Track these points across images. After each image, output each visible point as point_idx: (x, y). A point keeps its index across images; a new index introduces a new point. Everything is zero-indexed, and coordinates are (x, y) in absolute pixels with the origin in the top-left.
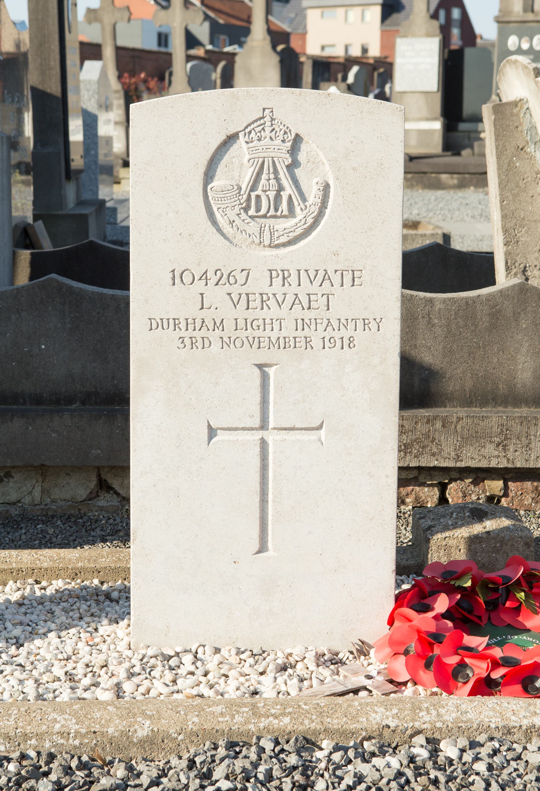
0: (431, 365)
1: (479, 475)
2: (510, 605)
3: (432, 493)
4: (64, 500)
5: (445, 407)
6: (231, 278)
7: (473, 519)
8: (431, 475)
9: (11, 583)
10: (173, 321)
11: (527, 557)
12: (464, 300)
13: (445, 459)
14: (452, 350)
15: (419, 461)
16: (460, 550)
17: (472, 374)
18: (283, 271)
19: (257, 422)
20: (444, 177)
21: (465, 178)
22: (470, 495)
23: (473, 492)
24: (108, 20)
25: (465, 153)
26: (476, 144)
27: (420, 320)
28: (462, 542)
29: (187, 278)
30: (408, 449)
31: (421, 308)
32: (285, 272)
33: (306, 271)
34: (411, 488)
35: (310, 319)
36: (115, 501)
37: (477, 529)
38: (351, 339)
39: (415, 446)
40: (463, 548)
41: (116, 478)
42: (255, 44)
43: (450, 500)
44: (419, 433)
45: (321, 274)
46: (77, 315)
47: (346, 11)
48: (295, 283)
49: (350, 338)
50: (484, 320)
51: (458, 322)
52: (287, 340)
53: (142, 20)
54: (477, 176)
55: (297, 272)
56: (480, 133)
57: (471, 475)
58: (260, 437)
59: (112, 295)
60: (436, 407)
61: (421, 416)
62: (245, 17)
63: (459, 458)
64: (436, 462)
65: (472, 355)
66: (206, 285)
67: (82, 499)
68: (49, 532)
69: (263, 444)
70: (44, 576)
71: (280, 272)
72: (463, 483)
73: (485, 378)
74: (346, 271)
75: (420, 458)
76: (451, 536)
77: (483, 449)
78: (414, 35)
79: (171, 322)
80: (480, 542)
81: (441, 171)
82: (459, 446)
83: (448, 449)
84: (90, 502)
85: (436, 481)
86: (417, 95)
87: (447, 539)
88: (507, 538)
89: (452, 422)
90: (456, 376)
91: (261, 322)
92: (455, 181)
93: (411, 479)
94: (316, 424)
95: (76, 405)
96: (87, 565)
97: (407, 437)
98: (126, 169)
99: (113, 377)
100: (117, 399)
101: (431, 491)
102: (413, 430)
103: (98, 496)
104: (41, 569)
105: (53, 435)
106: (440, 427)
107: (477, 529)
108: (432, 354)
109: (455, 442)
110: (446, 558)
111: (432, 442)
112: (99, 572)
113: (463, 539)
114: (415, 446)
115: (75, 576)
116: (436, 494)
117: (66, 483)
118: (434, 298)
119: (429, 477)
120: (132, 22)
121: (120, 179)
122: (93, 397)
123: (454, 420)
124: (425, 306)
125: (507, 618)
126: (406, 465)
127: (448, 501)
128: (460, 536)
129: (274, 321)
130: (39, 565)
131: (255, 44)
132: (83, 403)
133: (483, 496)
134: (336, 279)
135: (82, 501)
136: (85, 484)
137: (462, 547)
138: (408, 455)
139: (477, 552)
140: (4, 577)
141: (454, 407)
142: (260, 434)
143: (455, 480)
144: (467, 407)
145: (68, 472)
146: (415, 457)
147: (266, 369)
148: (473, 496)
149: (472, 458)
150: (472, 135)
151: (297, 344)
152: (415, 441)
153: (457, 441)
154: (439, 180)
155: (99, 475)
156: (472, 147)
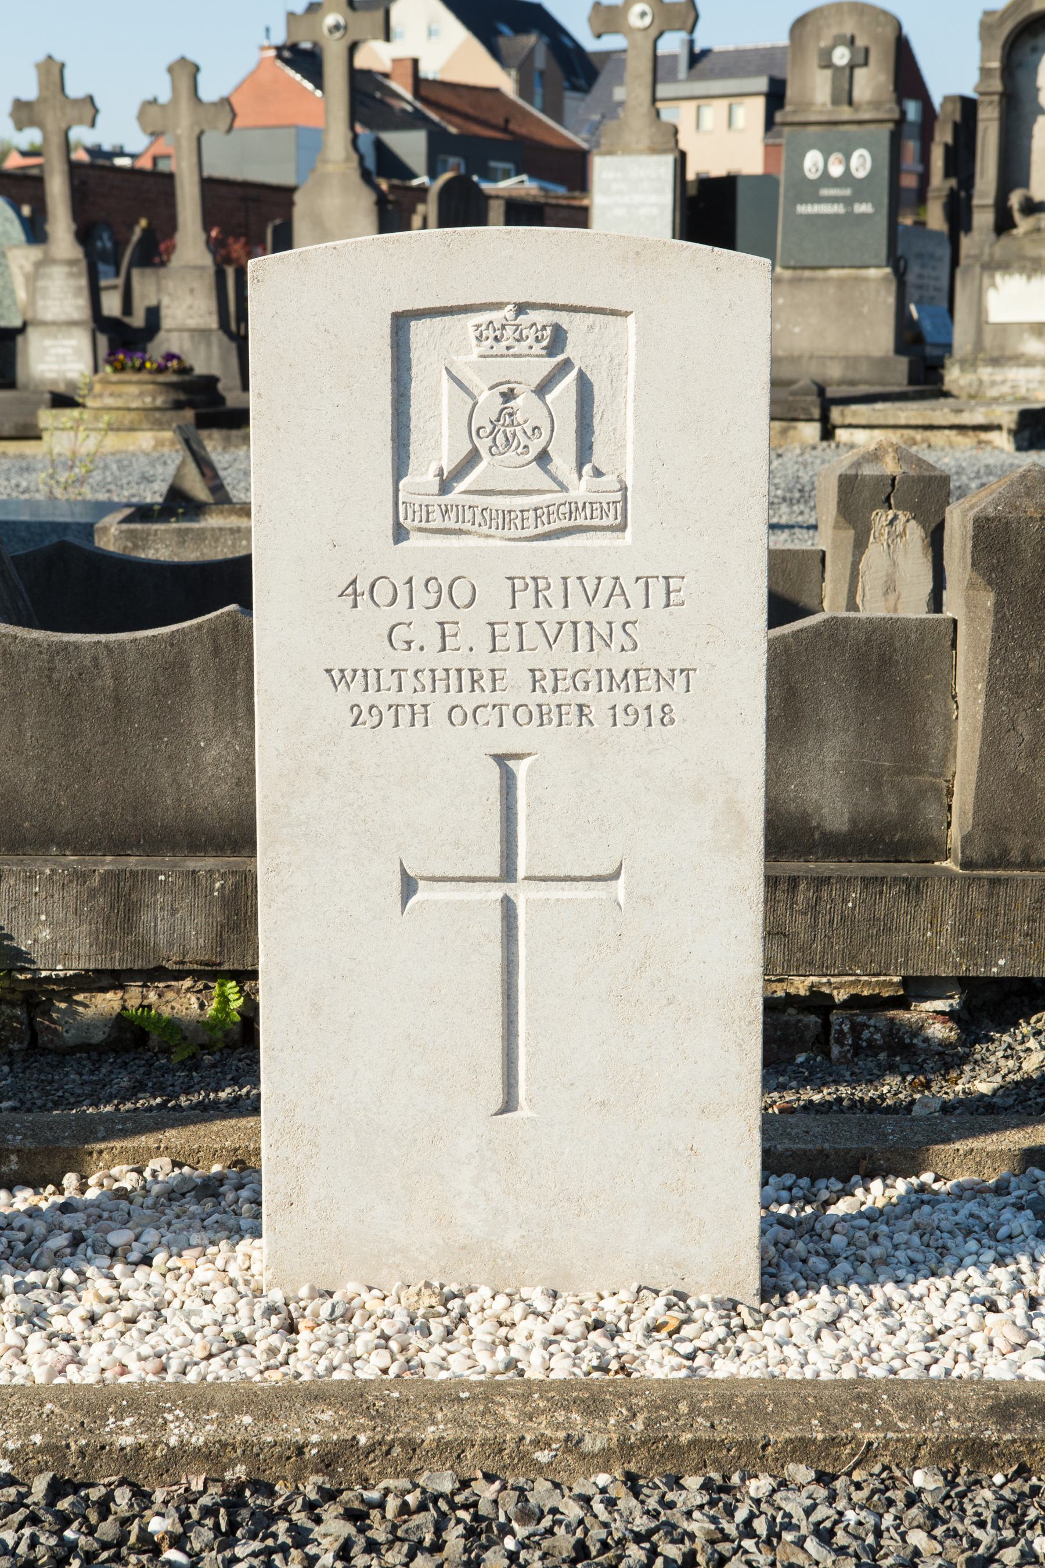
18: (535, 579)
19: (496, 872)
29: (383, 592)
35: (673, 671)
42: (330, 168)
45: (607, 585)
47: (698, 108)
48: (558, 602)
49: (664, 707)
52: (545, 709)
53: (297, 127)
55: (562, 581)
66: (355, 606)
69: (508, 907)
71: (529, 581)
74: (652, 577)
78: (628, 151)
79: (466, 674)
120: (233, 133)
121: (42, 430)
129: (677, 672)
131: (330, 168)
134: (636, 593)
142: (496, 892)
147: (511, 764)
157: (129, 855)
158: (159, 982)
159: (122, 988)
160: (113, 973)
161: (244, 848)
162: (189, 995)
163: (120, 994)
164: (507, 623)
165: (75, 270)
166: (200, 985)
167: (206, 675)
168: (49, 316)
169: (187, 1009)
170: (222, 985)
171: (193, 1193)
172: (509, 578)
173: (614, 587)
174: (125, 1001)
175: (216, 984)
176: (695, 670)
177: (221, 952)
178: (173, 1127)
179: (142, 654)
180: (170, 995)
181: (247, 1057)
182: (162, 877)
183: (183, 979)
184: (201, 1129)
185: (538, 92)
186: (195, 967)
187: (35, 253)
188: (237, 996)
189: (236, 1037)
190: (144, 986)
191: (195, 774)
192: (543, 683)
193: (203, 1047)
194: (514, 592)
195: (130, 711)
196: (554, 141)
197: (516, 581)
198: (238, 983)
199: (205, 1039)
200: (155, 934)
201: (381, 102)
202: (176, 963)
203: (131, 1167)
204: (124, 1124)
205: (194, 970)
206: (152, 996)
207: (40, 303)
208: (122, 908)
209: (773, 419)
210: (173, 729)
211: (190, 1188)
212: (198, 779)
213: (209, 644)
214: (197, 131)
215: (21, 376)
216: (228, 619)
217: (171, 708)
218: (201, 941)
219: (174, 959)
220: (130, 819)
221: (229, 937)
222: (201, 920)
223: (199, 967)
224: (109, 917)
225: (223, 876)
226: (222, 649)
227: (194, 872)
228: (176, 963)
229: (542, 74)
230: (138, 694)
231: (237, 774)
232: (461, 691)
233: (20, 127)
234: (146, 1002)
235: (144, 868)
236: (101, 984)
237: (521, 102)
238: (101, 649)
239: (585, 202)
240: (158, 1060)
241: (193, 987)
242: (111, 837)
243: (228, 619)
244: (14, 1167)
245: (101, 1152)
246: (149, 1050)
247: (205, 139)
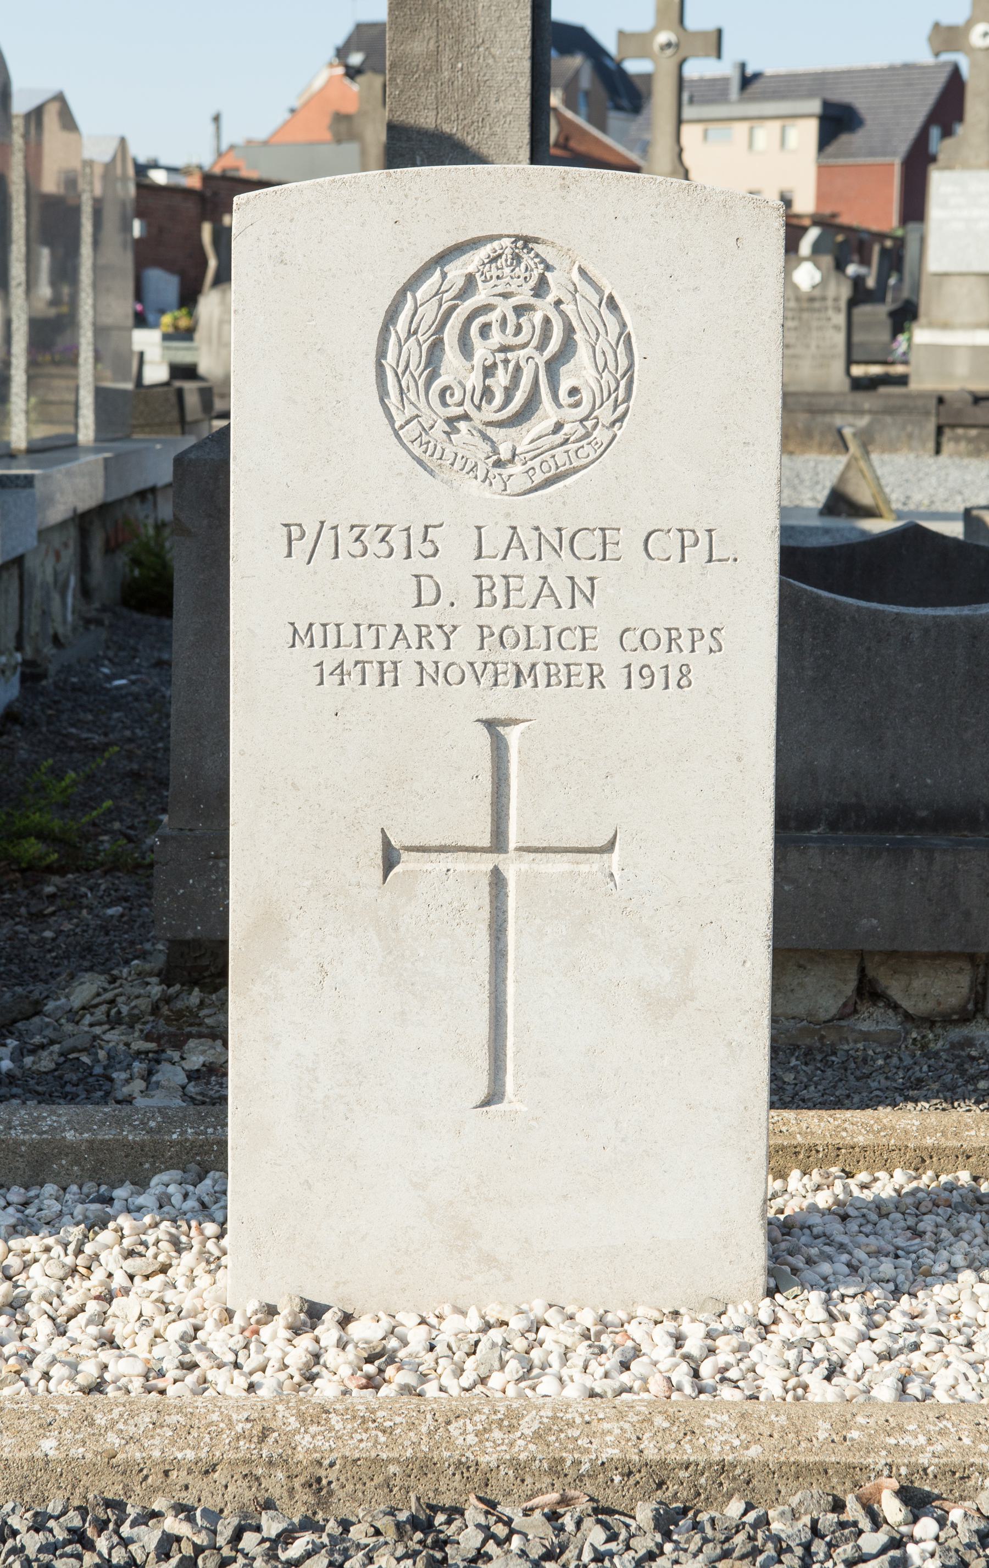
4: (793, 1018)
9: (795, 1174)
19: (486, 842)
36: (891, 1022)
41: (897, 976)
46: (828, 651)
58: (491, 867)
59: (897, 614)
67: (828, 1017)
68: (786, 1080)
69: (497, 880)
70: (858, 1162)
84: (843, 1023)
95: (820, 830)
96: (944, 1143)
99: (892, 777)
100: (899, 819)
103: (855, 1011)
104: (853, 1148)
105: (786, 888)
112: (968, 1157)
115: (919, 1164)
117: (799, 984)
122: (853, 815)
130: (848, 1140)
132: (833, 826)
135: (829, 1021)
136: (835, 985)
140: (781, 1162)
142: (486, 863)
145: (802, 962)
147: (500, 729)
151: (572, 678)
155: (862, 971)
164: (522, 577)
172: (286, 525)
173: (512, 540)
176: (385, 626)
185: (583, 109)
192: (429, 638)
194: (683, 548)
197: (292, 528)
229: (587, 94)
232: (325, 645)
239: (646, 136)
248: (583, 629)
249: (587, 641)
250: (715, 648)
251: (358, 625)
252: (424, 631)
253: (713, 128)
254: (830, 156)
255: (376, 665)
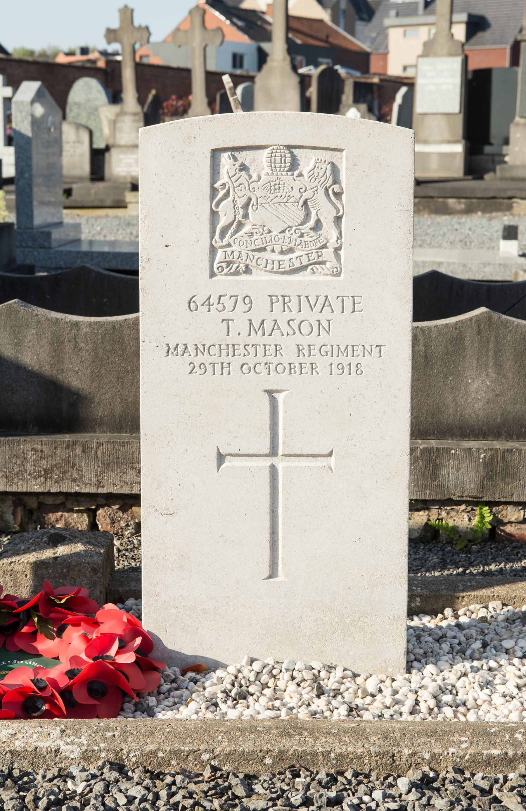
0: (79, 389)
1: (126, 501)
2: (28, 629)
3: (82, 519)
5: (95, 432)
6: (192, 304)
7: (48, 544)
8: (78, 501)
10: (351, 348)
11: (95, 583)
12: (110, 324)
13: (86, 485)
14: (100, 375)
15: (60, 486)
16: (26, 575)
17: (121, 400)
19: (267, 451)
20: (451, 202)
21: (472, 203)
22: (119, 521)
23: (121, 518)
24: (127, 39)
25: (488, 177)
26: (498, 168)
27: (67, 344)
28: (28, 567)
30: (48, 474)
31: (67, 332)
32: (273, 298)
33: (307, 297)
34: (60, 513)
37: (48, 554)
38: (359, 365)
39: (56, 472)
40: (29, 573)
42: (275, 64)
43: (100, 526)
44: (58, 458)
45: (321, 300)
49: (357, 364)
50: (132, 344)
51: (106, 346)
54: (485, 201)
56: (504, 156)
57: (118, 501)
58: (270, 464)
60: (85, 432)
61: (60, 441)
62: (324, 37)
63: (100, 483)
64: (77, 488)
65: (120, 380)
66: (209, 311)
72: (110, 509)
73: (134, 403)
75: (61, 484)
76: (17, 561)
77: (125, 475)
80: (46, 568)
81: (448, 195)
82: (100, 472)
83: (90, 475)
85: (83, 507)
86: (439, 116)
87: (12, 564)
88: (74, 564)
89: (92, 448)
90: (105, 401)
91: (329, 348)
92: (463, 206)
93: (58, 504)
94: (326, 452)
97: (47, 462)
98: (134, 194)
101: (81, 517)
102: (53, 455)
106: (80, 452)
107: (48, 554)
108: (80, 379)
109: (96, 468)
110: (12, 583)
111: (73, 467)
113: (29, 565)
114: (56, 472)
116: (85, 521)
118: (79, 322)
119: (76, 503)
121: (127, 203)
123: (95, 445)
124: (71, 330)
125: (20, 644)
126: (46, 491)
127: (98, 527)
128: (26, 561)
133: (132, 522)
134: (337, 305)
137: (28, 572)
138: (48, 480)
139: (44, 578)
141: (104, 433)
142: (267, 462)
143: (103, 506)
144: (117, 432)
146: (56, 482)
148: (122, 522)
149: (114, 484)
150: (497, 159)
152: (55, 466)
153: (98, 466)
154: (446, 205)
156: (494, 170)
157: (429, 439)
158: (448, 506)
159: (428, 509)
160: (424, 502)
161: (489, 436)
162: (463, 514)
163: (427, 512)
165: (137, 118)
166: (469, 508)
167: (473, 345)
168: (123, 142)
169: (462, 521)
170: (481, 509)
171: (519, 620)
174: (429, 516)
175: (478, 508)
177: (482, 491)
178: (497, 585)
179: (440, 333)
180: (453, 514)
181: (494, 547)
182: (453, 451)
183: (460, 505)
184: (513, 586)
185: (342, 21)
186: (468, 499)
187: (115, 109)
188: (489, 515)
189: (487, 536)
190: (440, 508)
191: (465, 397)
193: (470, 541)
195: (433, 363)
196: (353, 48)
198: (489, 507)
199: (470, 537)
200: (448, 481)
201: (261, 27)
202: (458, 497)
203: (482, 606)
204: (471, 582)
205: (468, 501)
206: (444, 514)
207: (118, 135)
208: (431, 467)
209: (415, 197)
210: (455, 373)
211: (517, 617)
212: (466, 399)
213: (475, 328)
214: (203, 45)
215: (107, 174)
216: (486, 315)
217: (454, 362)
218: (472, 485)
219: (458, 494)
220: (430, 420)
221: (487, 484)
222: (472, 474)
223: (471, 499)
224: (424, 472)
225: (485, 451)
226: (482, 331)
227: (470, 449)
228: (458, 497)
229: (344, 12)
230: (437, 354)
231: (487, 397)
233: (109, 42)
234: (440, 517)
235: (443, 446)
236: (417, 507)
237: (334, 26)
238: (419, 331)
240: (446, 548)
241: (466, 509)
242: (419, 430)
243: (486, 315)
244: (418, 604)
245: (463, 597)
246: (440, 542)
247: (208, 49)
248: (265, 345)
249: (236, 351)
250: (246, 353)
251: (371, 346)
252: (301, 347)
253: (409, 30)
254: (472, 45)
255: (220, 365)
